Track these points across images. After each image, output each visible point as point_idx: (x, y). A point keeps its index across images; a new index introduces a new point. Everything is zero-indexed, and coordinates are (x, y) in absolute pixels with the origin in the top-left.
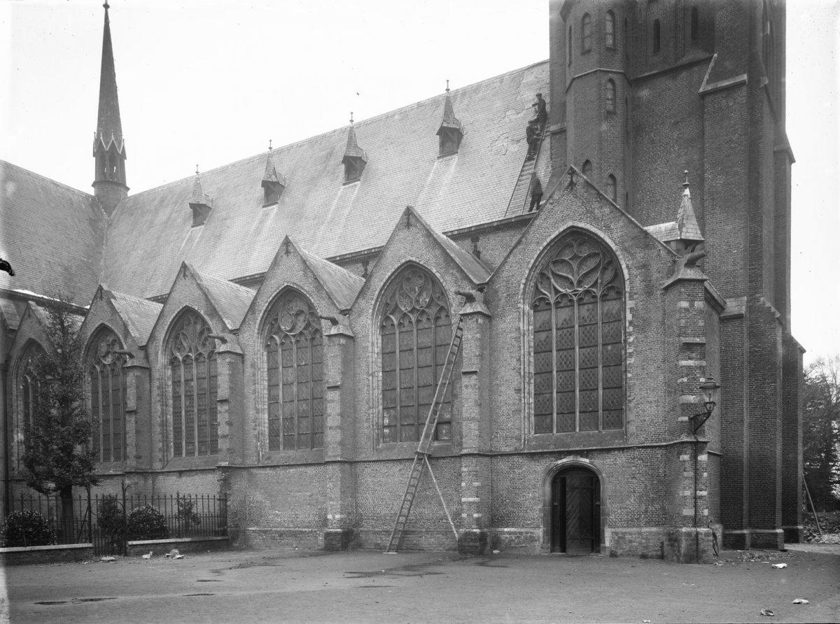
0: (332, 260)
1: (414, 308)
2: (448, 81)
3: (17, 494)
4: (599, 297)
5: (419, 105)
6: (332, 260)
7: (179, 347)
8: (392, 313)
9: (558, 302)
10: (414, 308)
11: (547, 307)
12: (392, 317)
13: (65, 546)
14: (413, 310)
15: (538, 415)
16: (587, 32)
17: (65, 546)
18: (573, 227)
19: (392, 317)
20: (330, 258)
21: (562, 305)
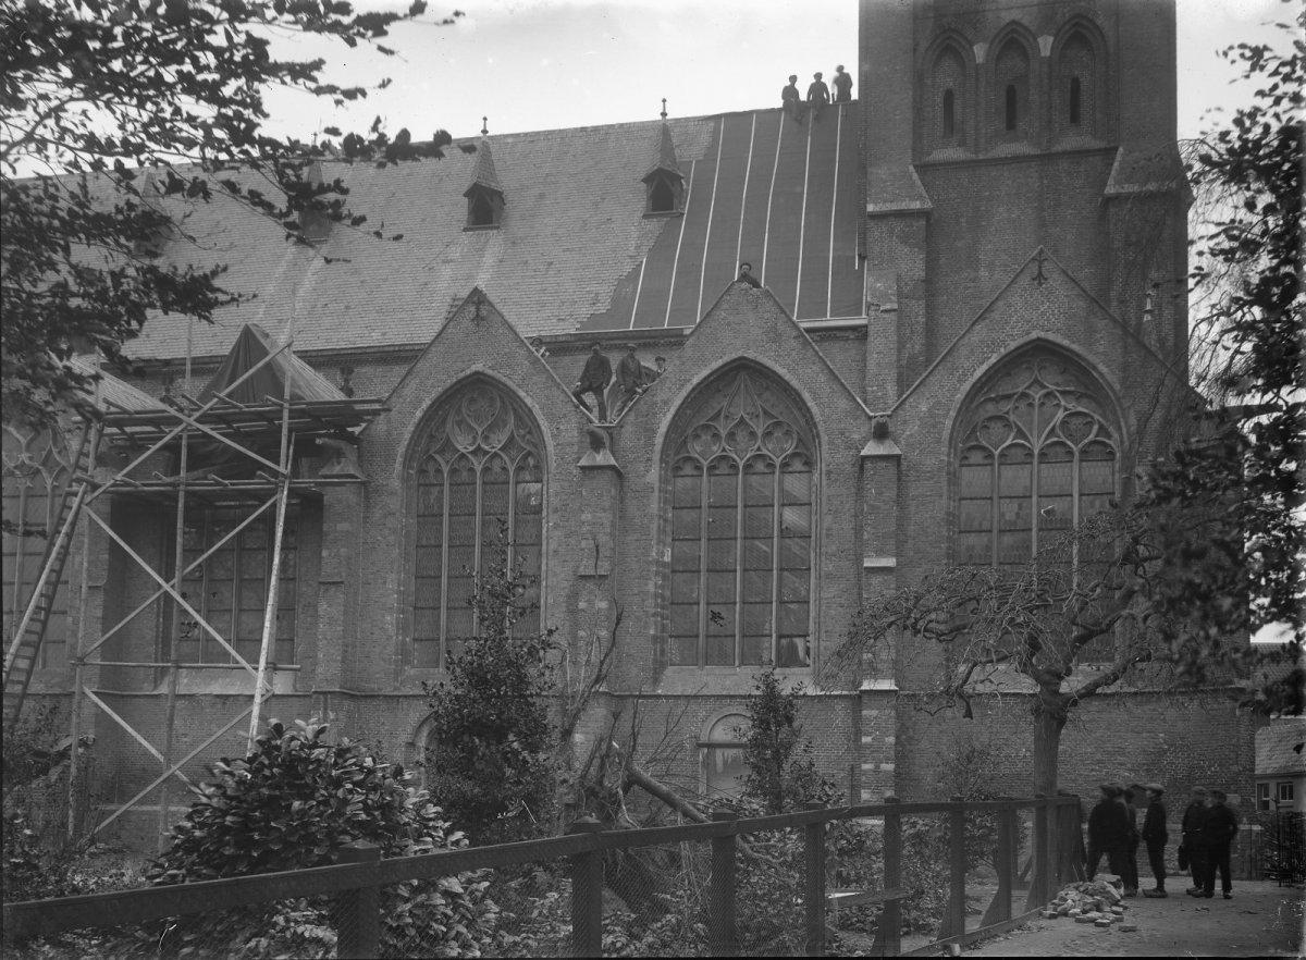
0: (305, 356)
1: (479, 448)
2: (664, 101)
3: (432, 489)
4: (741, 468)
5: (583, 129)
6: (305, 356)
7: (688, 516)
8: (441, 452)
9: (714, 467)
10: (479, 448)
11: (731, 472)
12: (437, 457)
13: (240, 527)
14: (478, 451)
15: (711, 571)
16: (291, 569)
17: (240, 527)
18: (1038, 339)
19: (437, 457)
20: (298, 351)
21: (717, 472)
